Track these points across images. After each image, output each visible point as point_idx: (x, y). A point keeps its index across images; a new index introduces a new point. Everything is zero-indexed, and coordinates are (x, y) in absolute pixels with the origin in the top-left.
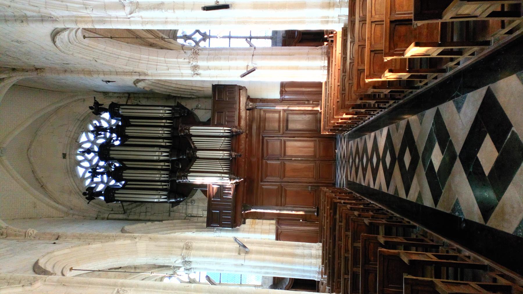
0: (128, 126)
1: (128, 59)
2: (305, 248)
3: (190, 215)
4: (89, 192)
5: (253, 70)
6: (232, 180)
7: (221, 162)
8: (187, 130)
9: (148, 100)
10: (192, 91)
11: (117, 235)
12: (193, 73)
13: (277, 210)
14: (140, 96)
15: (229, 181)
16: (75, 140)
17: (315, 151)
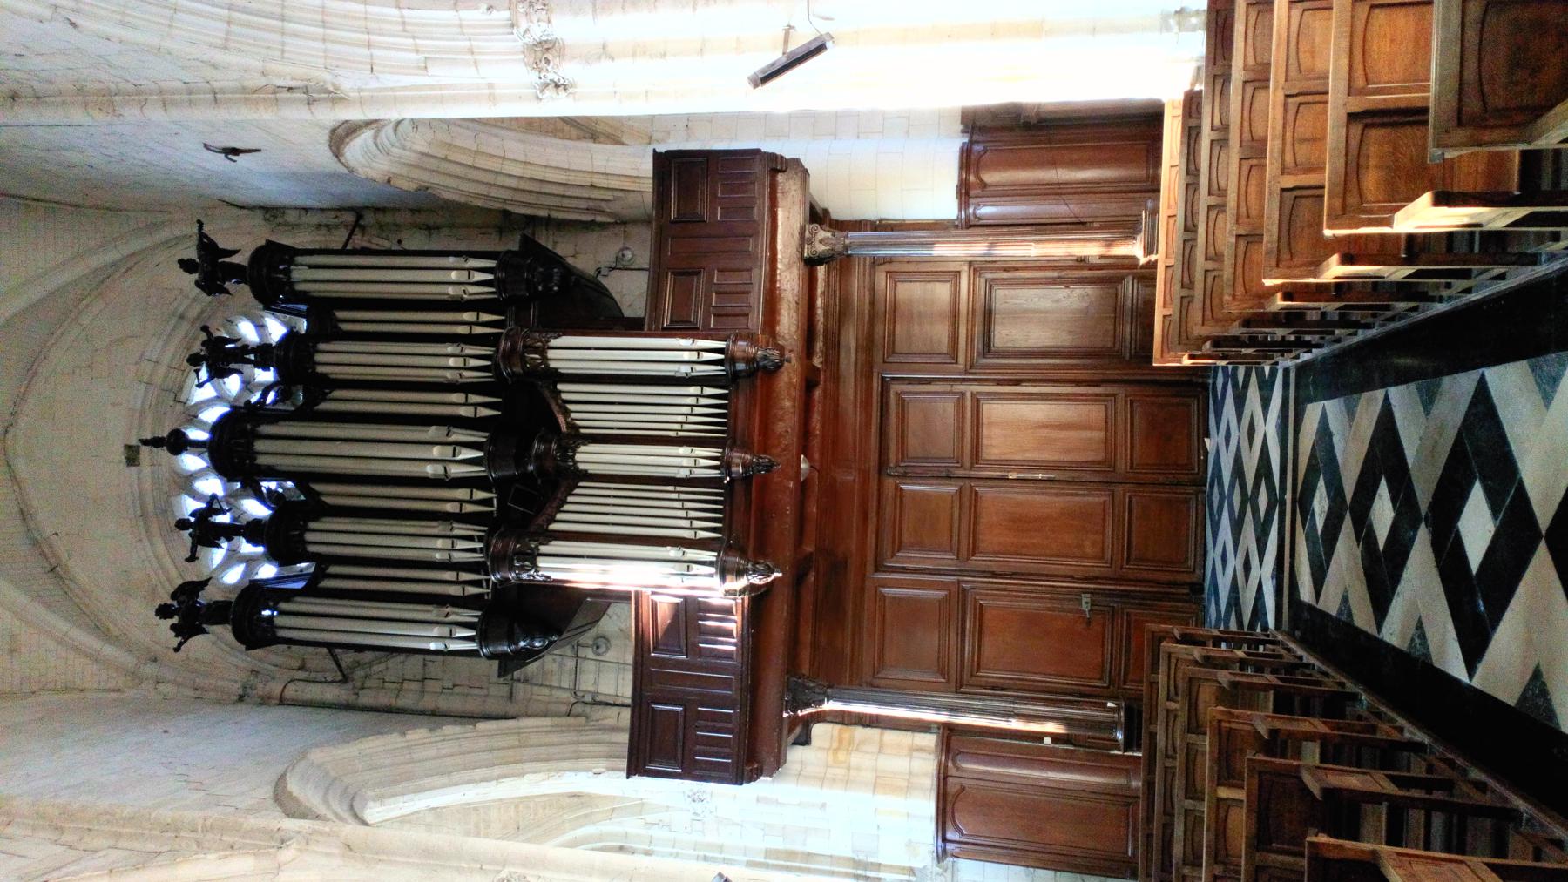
0: (328, 340)
1: (225, 12)
3: (588, 699)
4: (179, 603)
6: (729, 577)
7: (683, 496)
8: (536, 350)
9: (430, 234)
10: (595, 194)
11: (208, 823)
12: (533, 76)
13: (938, 708)
14: (399, 218)
16: (172, 395)
17: (1109, 444)
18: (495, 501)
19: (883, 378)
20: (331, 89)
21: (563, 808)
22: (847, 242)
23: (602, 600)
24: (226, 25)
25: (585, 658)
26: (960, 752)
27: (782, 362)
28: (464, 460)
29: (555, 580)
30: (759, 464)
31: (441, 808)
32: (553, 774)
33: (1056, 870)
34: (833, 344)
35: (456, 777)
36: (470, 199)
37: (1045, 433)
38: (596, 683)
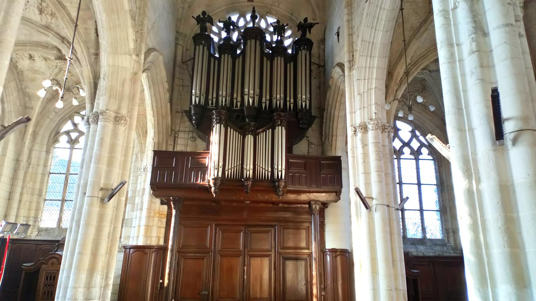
0: (284, 60)
1: (372, 41)
2: (102, 288)
3: (176, 135)
4: (206, 18)
5: (367, 207)
7: (238, 167)
8: (281, 123)
10: (330, 136)
11: (144, 34)
12: (357, 125)
13: (172, 246)
15: (212, 177)
16: (269, 11)
18: (237, 108)
19: (276, 226)
20: (353, 68)
21: (143, 128)
22: (316, 215)
23: (208, 143)
24: (368, 41)
25: (189, 134)
26: (158, 253)
27: (278, 196)
28: (249, 100)
29: (213, 129)
30: (248, 189)
31: (144, 93)
32: (154, 126)
33: (120, 284)
34: (286, 210)
35: (154, 98)
36: (327, 100)
37: (259, 277)
38: (181, 138)
